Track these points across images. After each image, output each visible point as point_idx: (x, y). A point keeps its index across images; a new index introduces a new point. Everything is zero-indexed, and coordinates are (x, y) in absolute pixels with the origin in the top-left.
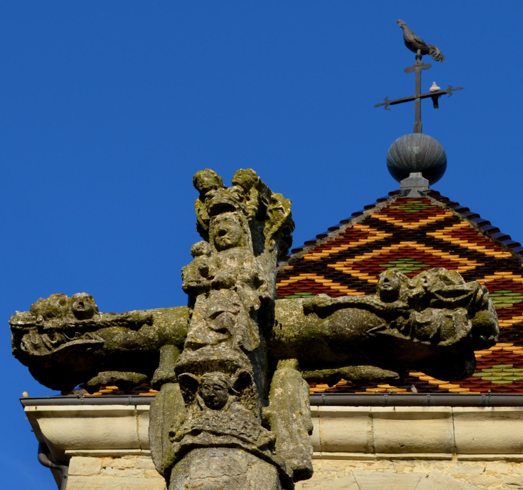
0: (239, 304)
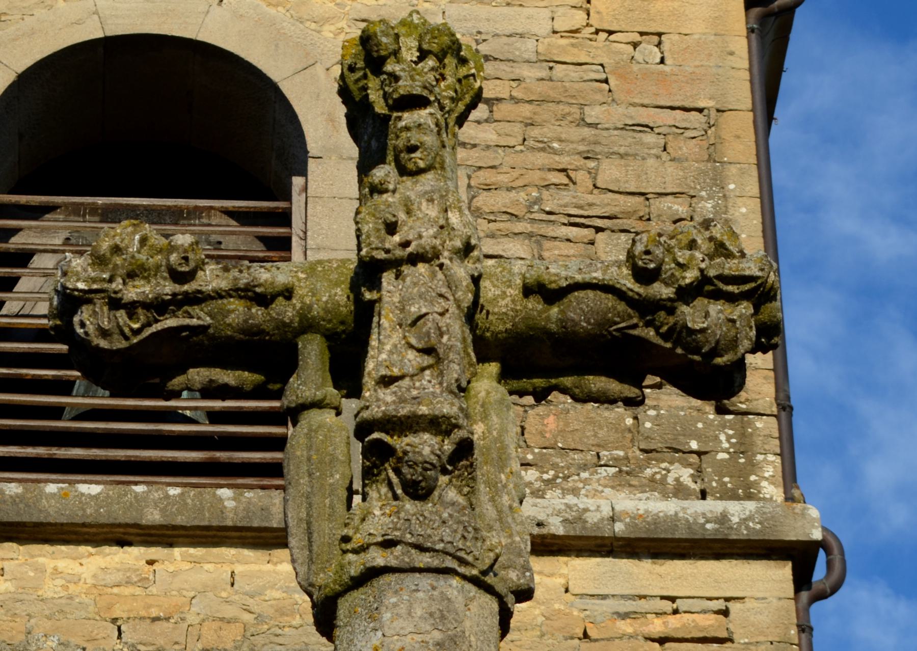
0: (447, 295)
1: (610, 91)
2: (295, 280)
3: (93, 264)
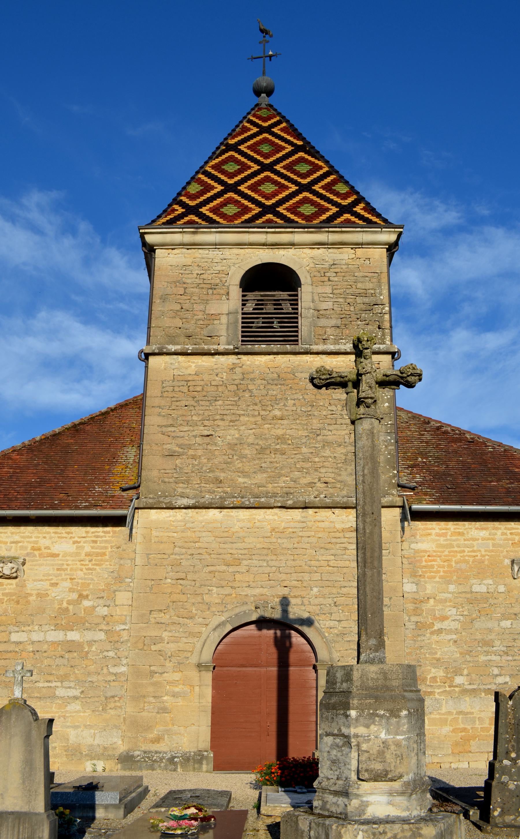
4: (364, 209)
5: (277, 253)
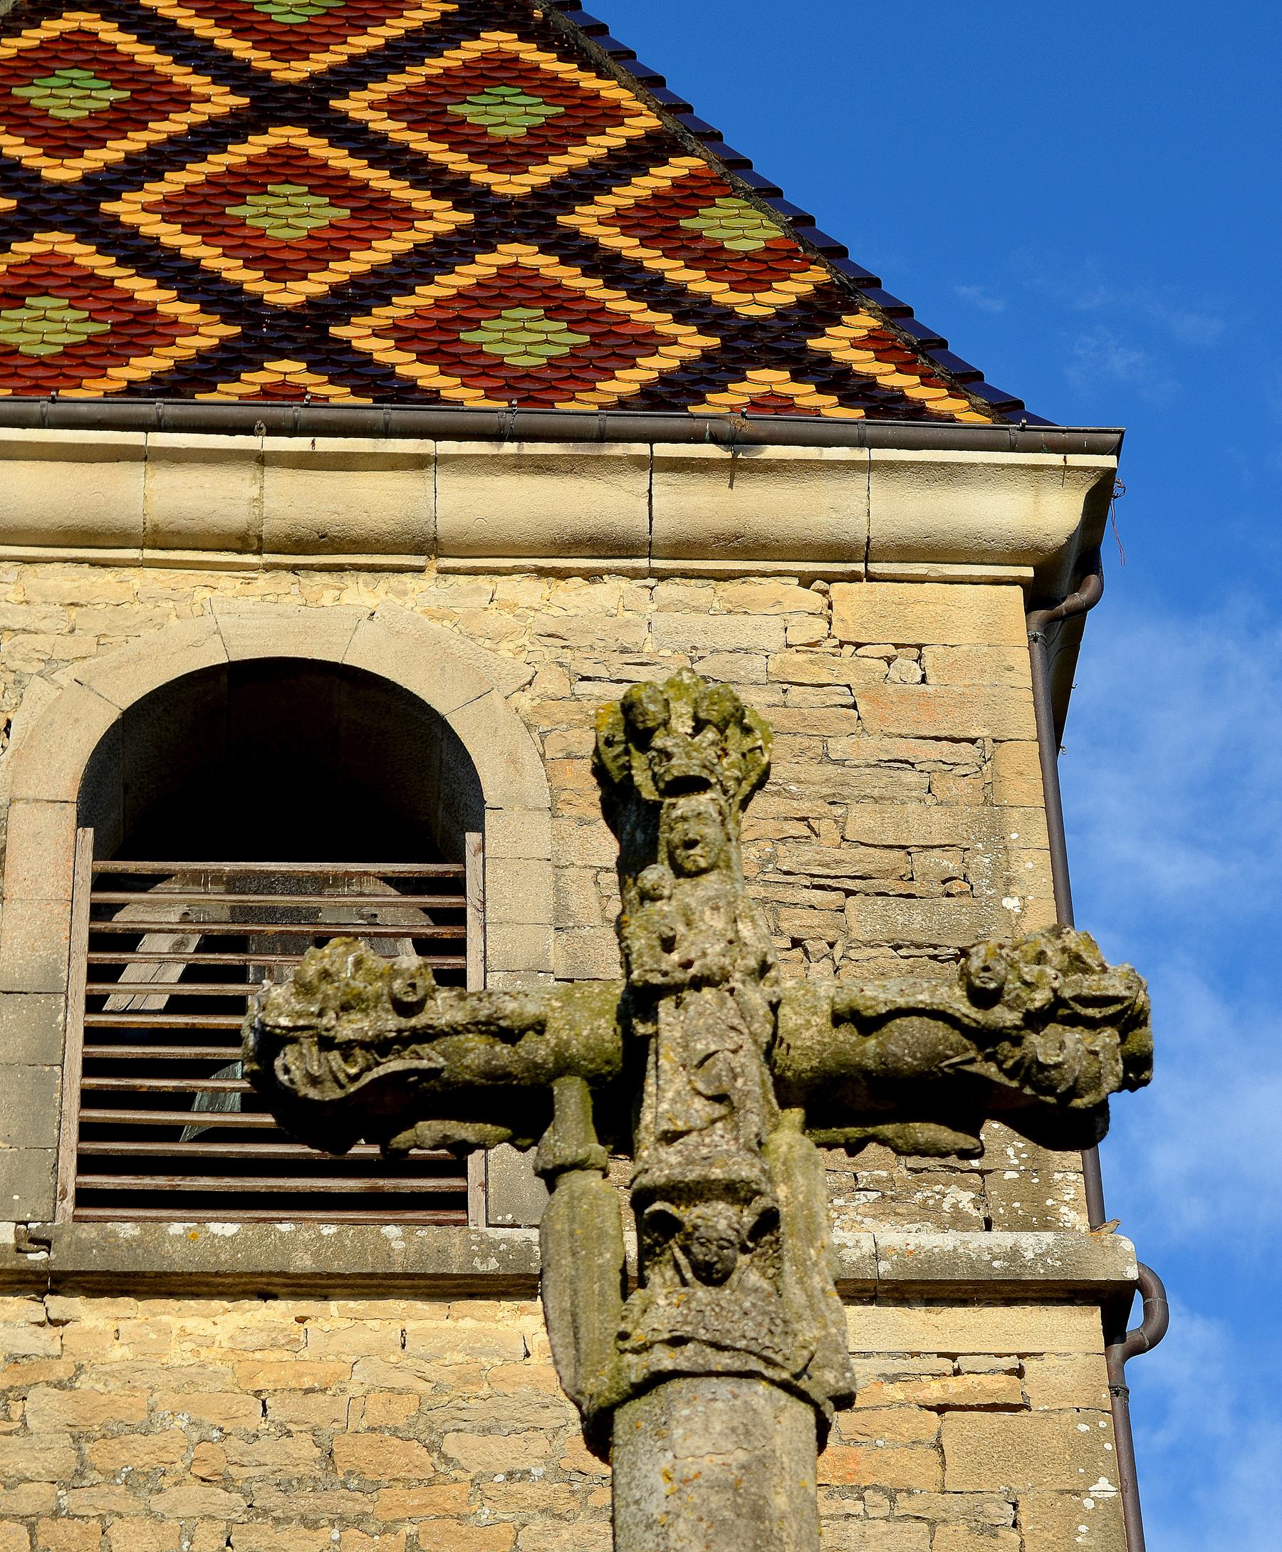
0: (740, 1027)
1: (859, 718)
2: (548, 1009)
3: (297, 993)
4: (874, 342)
5: (328, 598)
